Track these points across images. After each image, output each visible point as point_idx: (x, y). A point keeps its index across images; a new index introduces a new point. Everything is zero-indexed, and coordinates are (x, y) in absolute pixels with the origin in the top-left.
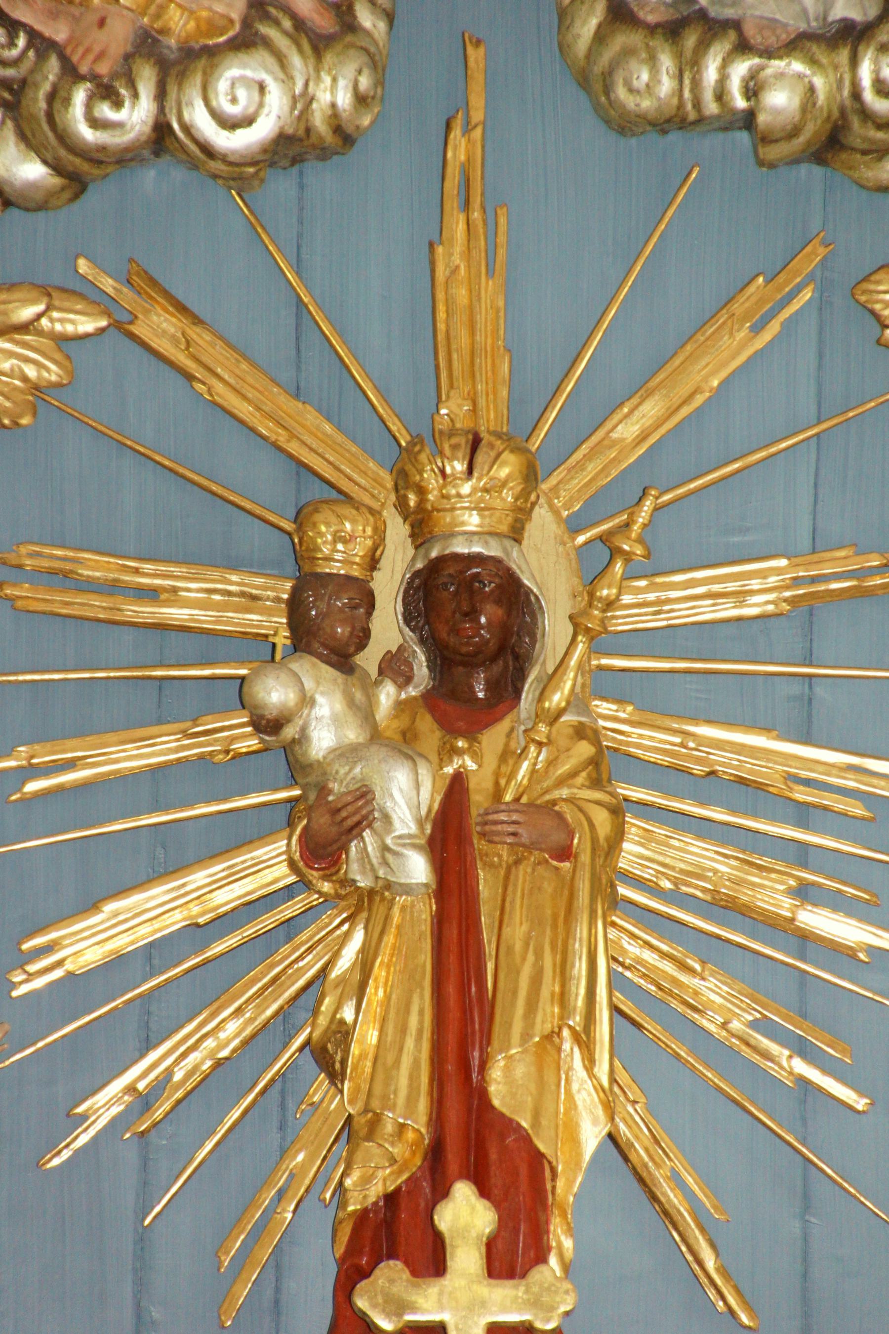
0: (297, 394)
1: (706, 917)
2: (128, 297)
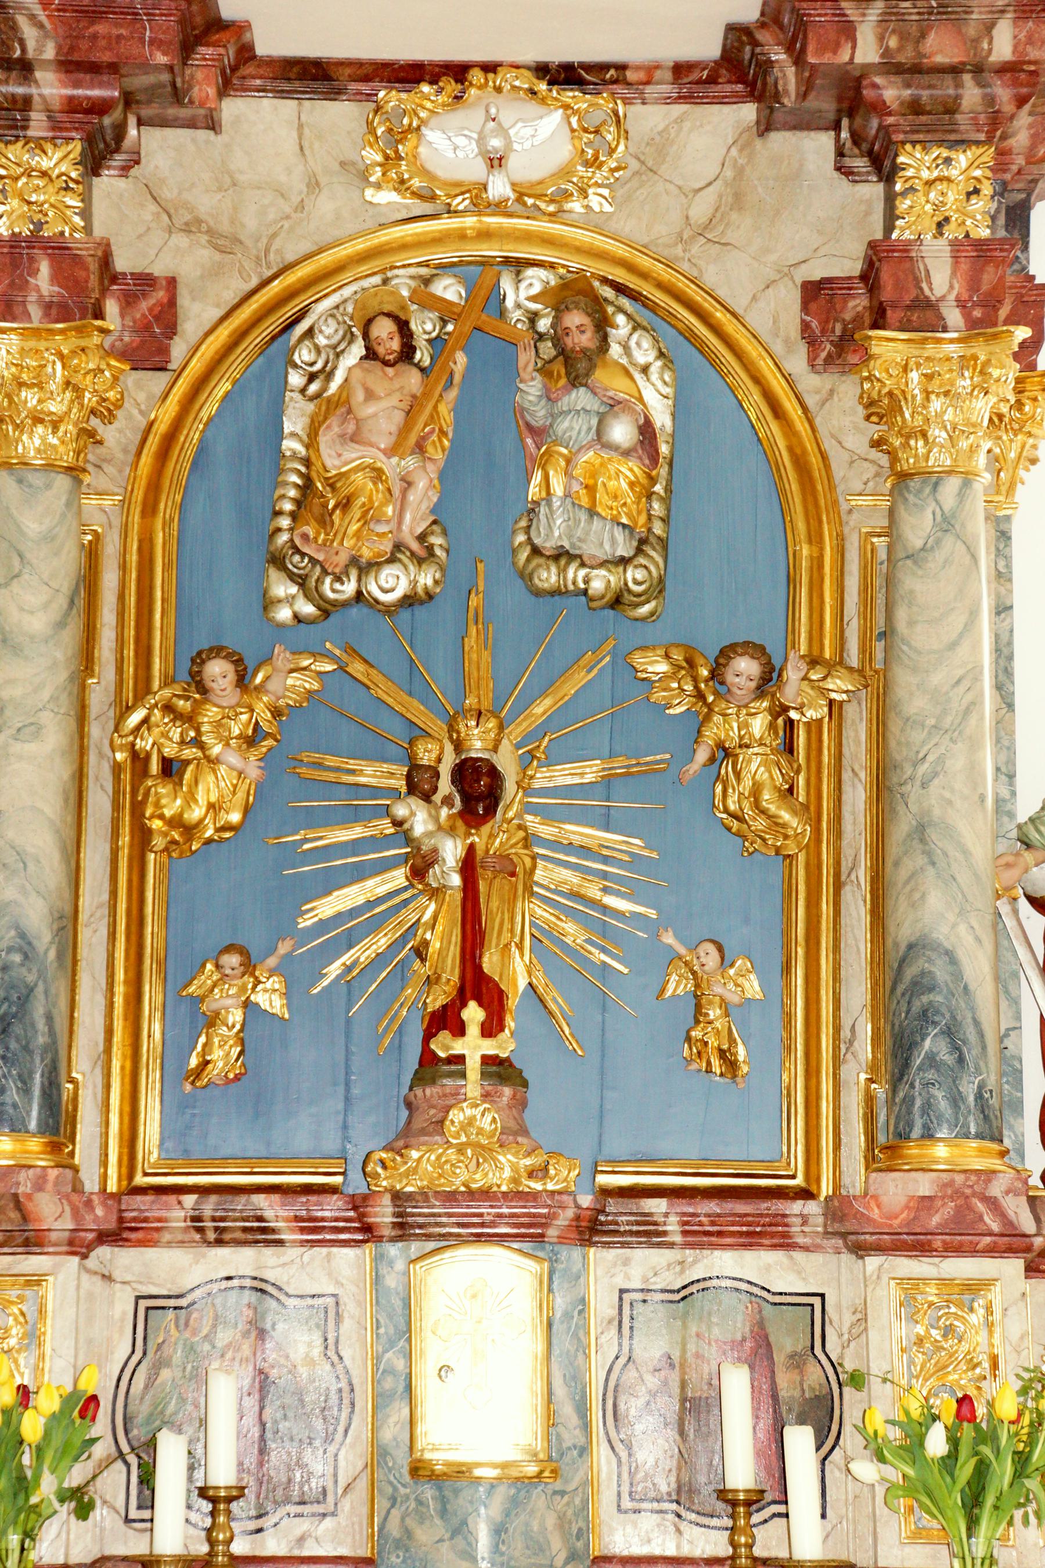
0: (410, 694)
1: (568, 899)
2: (345, 657)
